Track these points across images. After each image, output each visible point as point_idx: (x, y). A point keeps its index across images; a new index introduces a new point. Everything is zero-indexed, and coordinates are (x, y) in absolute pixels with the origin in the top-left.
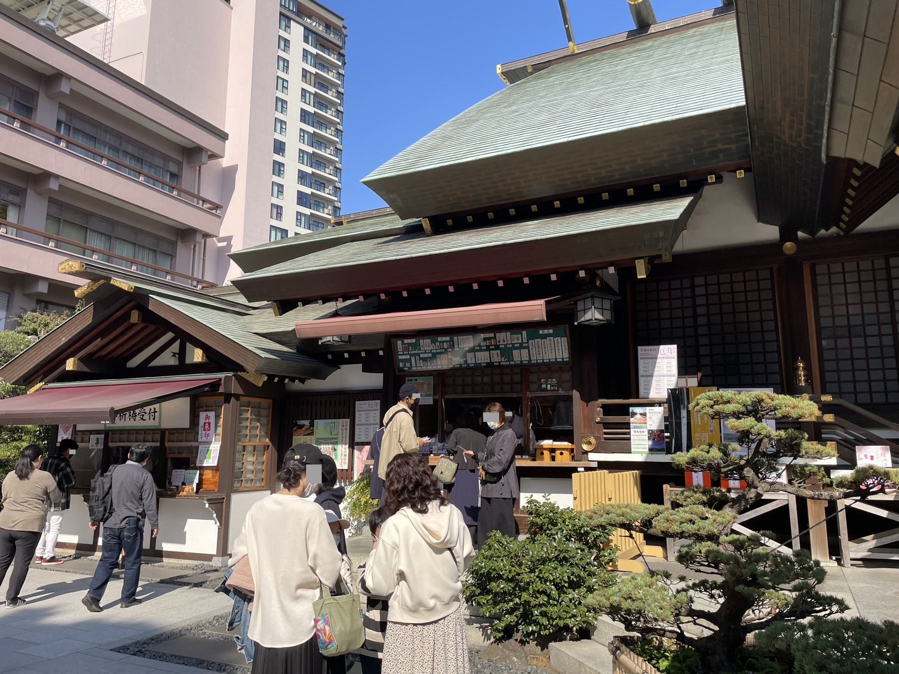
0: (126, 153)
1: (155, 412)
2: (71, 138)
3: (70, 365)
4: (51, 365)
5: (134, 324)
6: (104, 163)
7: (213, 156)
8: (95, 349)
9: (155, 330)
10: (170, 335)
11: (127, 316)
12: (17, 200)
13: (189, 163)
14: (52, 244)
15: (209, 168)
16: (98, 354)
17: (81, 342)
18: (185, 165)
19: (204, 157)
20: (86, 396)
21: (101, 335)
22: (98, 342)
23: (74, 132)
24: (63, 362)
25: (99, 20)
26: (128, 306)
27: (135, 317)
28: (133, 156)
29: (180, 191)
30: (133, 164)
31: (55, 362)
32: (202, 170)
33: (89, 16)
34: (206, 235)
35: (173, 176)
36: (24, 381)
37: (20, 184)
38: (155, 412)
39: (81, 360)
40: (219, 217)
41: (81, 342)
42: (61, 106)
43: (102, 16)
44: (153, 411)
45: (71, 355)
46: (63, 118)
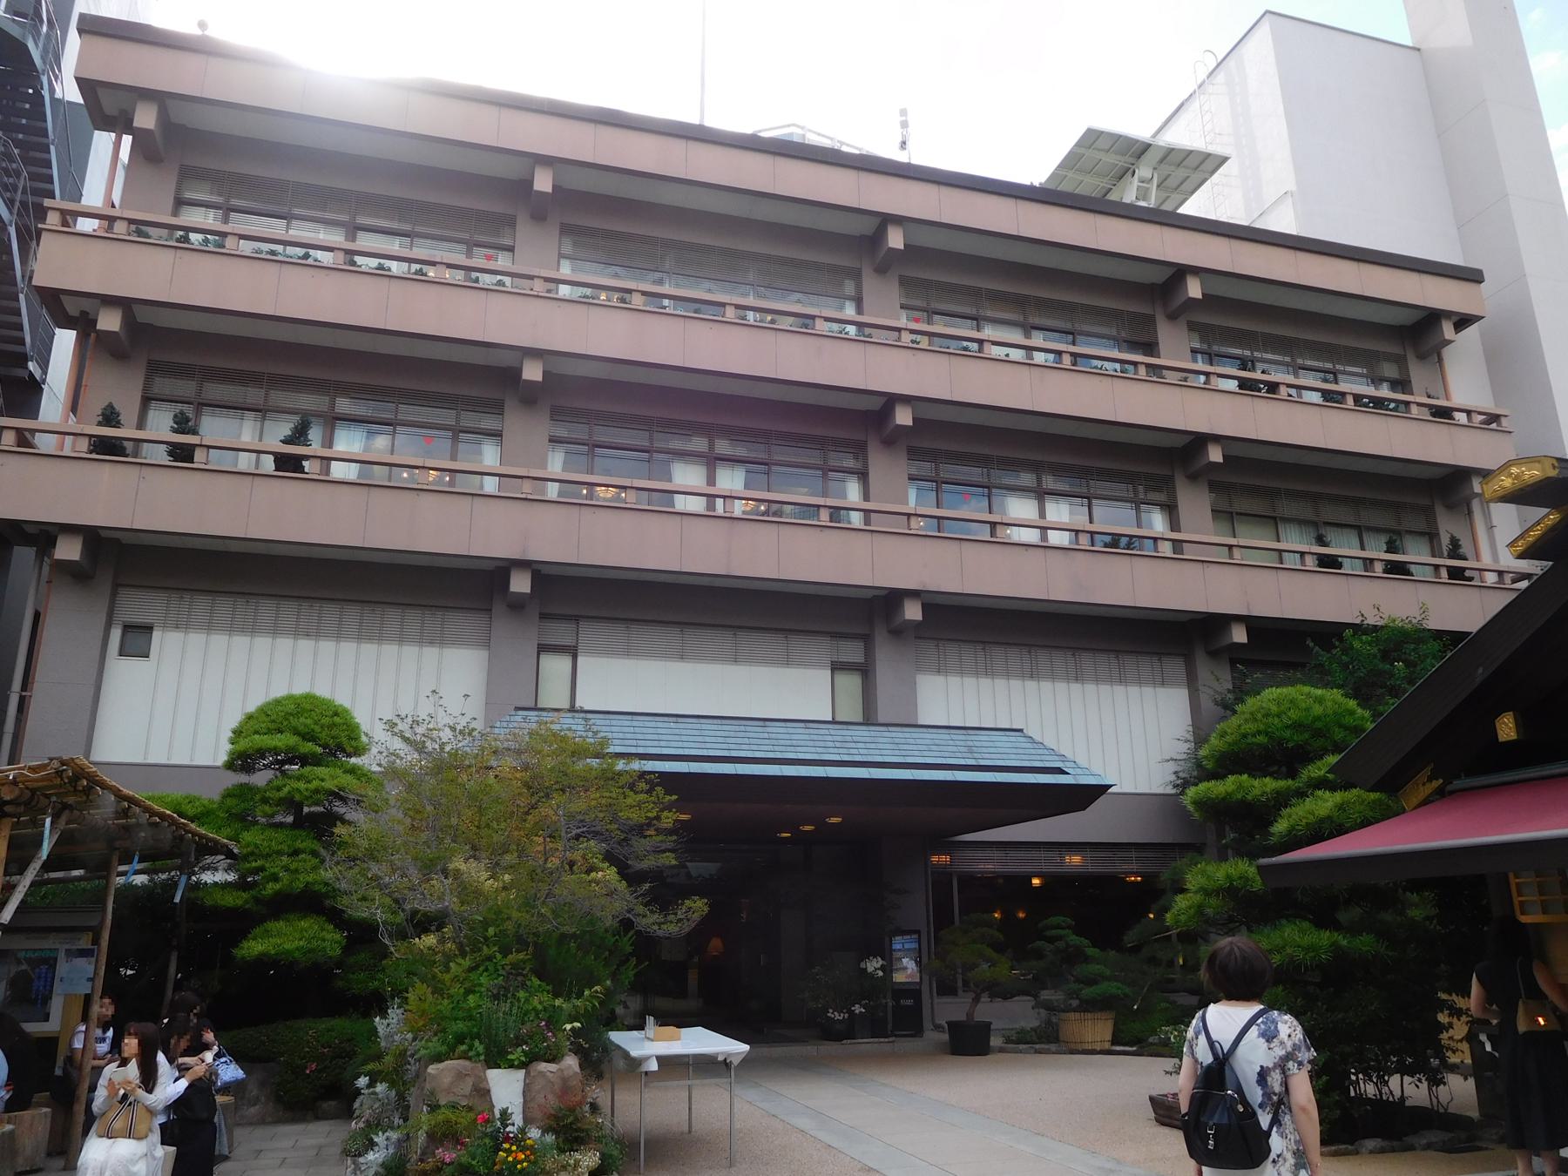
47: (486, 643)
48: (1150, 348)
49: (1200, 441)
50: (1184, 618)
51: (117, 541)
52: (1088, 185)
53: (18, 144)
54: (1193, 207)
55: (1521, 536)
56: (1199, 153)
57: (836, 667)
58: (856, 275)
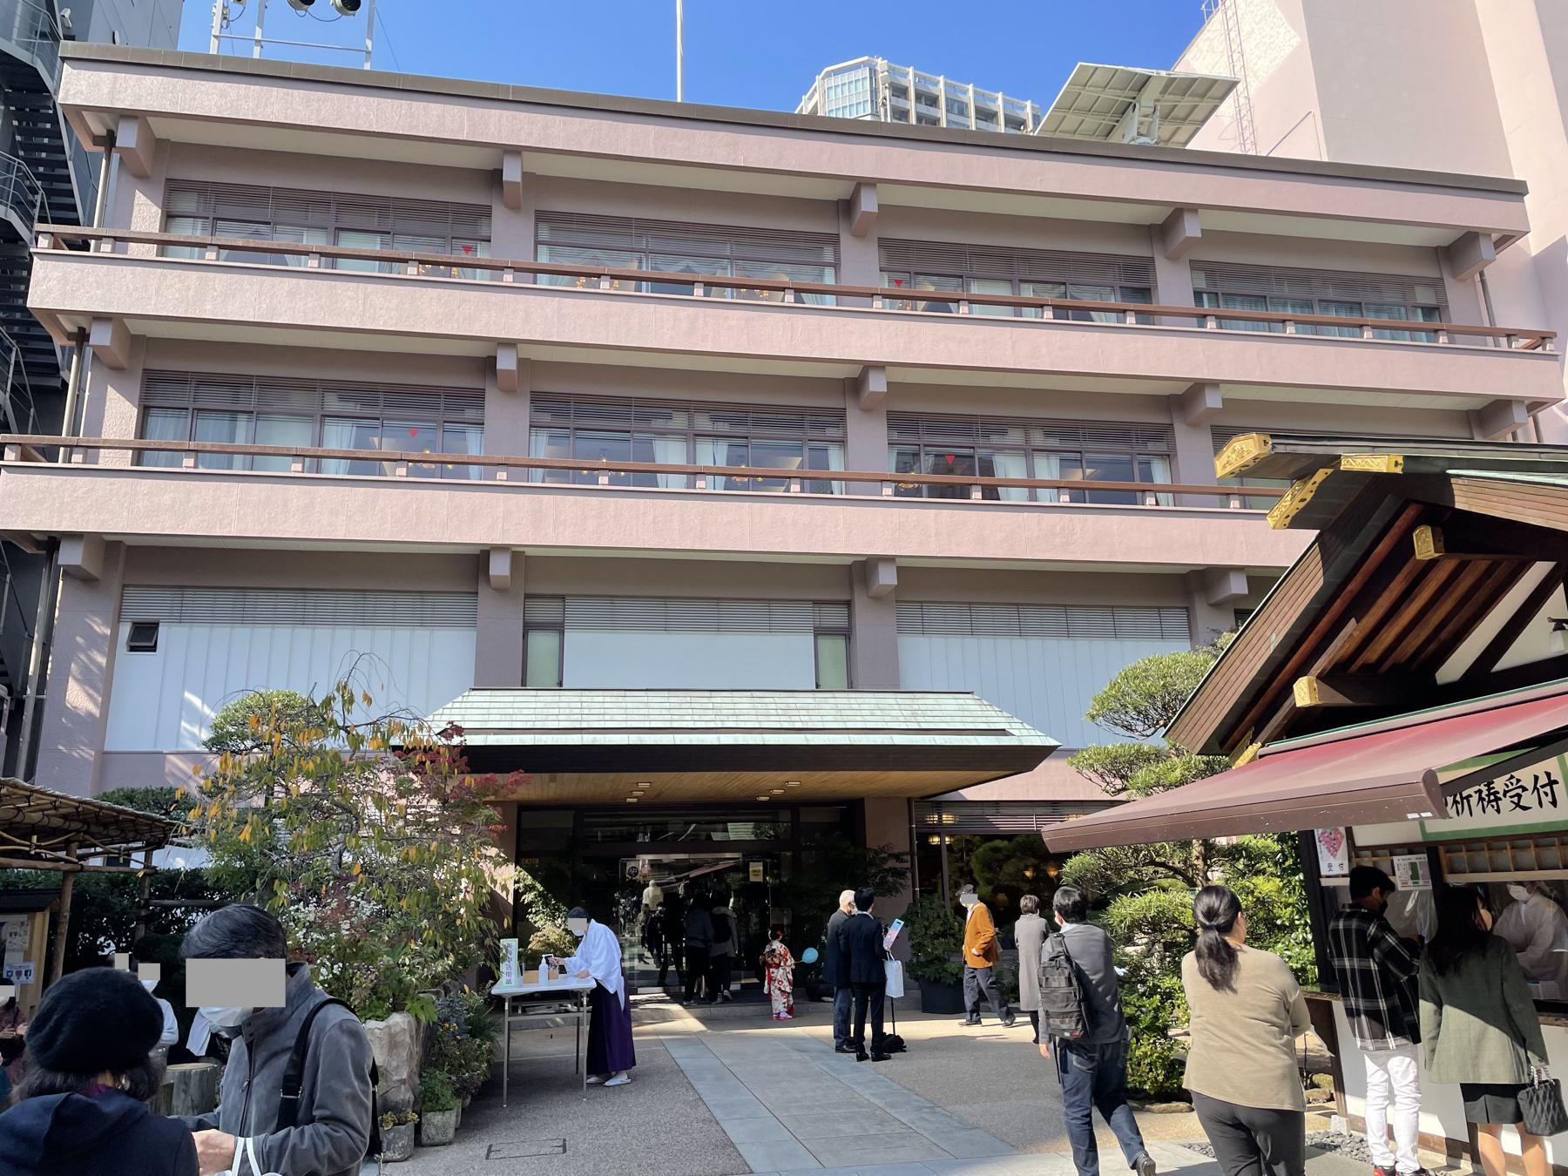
0: (1326, 303)
1: (1552, 783)
2: (1223, 310)
3: (1304, 693)
4: (1263, 702)
5: (1431, 564)
6: (1290, 330)
7: (1505, 239)
8: (1351, 647)
9: (1488, 572)
10: (1539, 571)
11: (1404, 548)
12: (1162, 447)
13: (1454, 276)
14: (1235, 504)
15: (1502, 268)
16: (1360, 662)
17: (1313, 638)
18: (1448, 281)
19: (1485, 247)
20: (1355, 757)
21: (1356, 608)
22: (1352, 631)
23: (1226, 303)
24: (1287, 690)
25: (1219, 94)
26: (1401, 523)
27: (1425, 545)
28: (1340, 304)
29: (1450, 332)
30: (1343, 316)
31: (1270, 693)
32: (1487, 277)
33: (1203, 96)
34: (1535, 406)
35: (1429, 311)
36: (1222, 744)
37: (1159, 419)
38: (1552, 783)
39: (1325, 678)
40: (1553, 357)
41: (1313, 638)
42: (1195, 265)
43: (1224, 81)
44: (1543, 780)
45: (1301, 671)
46: (1202, 284)
47: (472, 622)
48: (1145, 293)
49: (1199, 387)
50: (1185, 570)
51: (120, 542)
52: (1086, 128)
53: (39, 176)
54: (1206, 140)
55: (39, 705)
56: (1204, 79)
57: (820, 632)
58: (834, 240)
